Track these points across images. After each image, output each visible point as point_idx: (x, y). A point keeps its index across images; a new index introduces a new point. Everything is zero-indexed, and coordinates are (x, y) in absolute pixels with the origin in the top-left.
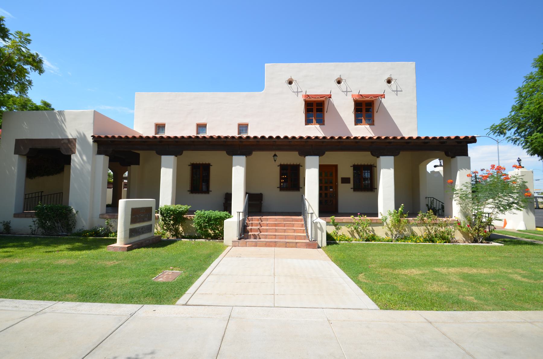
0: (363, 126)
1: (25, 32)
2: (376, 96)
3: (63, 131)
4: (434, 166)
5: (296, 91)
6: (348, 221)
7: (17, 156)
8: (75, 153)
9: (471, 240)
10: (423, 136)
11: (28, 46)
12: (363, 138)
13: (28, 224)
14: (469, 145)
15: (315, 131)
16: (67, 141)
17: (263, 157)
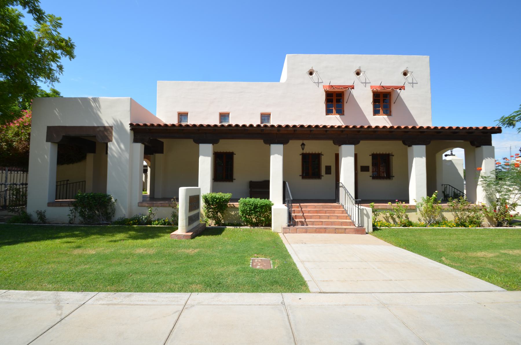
0: (334, 116)
1: (57, 16)
2: (346, 87)
3: (98, 118)
4: (457, 156)
5: (317, 81)
6: (383, 207)
7: (49, 143)
8: (111, 141)
9: (495, 224)
10: (439, 126)
11: (59, 30)
12: (332, 127)
13: (63, 213)
14: (492, 135)
15: (335, 121)
16: (103, 129)
17: (295, 145)
